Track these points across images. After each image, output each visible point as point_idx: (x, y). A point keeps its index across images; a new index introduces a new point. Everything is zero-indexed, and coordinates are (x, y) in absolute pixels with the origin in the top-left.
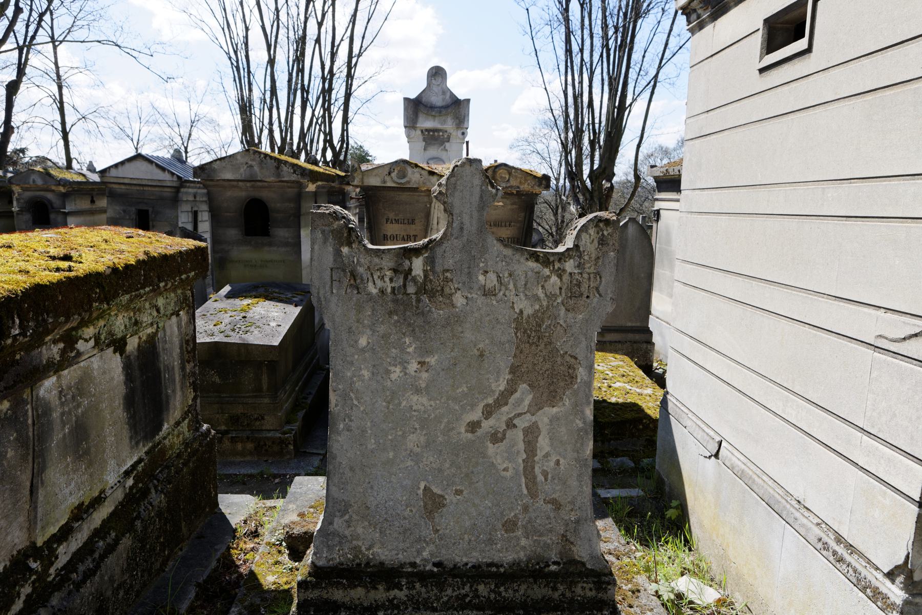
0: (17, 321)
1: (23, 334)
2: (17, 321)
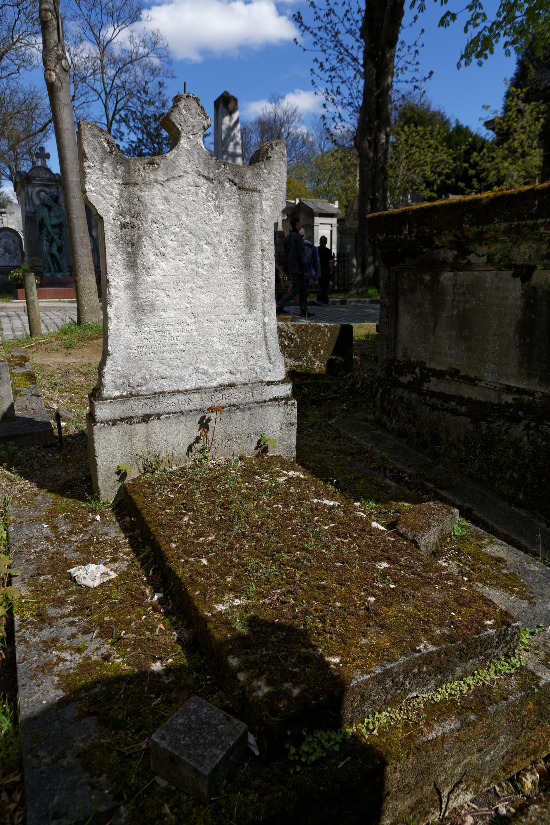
0: (407, 227)
1: (410, 233)
2: (407, 227)
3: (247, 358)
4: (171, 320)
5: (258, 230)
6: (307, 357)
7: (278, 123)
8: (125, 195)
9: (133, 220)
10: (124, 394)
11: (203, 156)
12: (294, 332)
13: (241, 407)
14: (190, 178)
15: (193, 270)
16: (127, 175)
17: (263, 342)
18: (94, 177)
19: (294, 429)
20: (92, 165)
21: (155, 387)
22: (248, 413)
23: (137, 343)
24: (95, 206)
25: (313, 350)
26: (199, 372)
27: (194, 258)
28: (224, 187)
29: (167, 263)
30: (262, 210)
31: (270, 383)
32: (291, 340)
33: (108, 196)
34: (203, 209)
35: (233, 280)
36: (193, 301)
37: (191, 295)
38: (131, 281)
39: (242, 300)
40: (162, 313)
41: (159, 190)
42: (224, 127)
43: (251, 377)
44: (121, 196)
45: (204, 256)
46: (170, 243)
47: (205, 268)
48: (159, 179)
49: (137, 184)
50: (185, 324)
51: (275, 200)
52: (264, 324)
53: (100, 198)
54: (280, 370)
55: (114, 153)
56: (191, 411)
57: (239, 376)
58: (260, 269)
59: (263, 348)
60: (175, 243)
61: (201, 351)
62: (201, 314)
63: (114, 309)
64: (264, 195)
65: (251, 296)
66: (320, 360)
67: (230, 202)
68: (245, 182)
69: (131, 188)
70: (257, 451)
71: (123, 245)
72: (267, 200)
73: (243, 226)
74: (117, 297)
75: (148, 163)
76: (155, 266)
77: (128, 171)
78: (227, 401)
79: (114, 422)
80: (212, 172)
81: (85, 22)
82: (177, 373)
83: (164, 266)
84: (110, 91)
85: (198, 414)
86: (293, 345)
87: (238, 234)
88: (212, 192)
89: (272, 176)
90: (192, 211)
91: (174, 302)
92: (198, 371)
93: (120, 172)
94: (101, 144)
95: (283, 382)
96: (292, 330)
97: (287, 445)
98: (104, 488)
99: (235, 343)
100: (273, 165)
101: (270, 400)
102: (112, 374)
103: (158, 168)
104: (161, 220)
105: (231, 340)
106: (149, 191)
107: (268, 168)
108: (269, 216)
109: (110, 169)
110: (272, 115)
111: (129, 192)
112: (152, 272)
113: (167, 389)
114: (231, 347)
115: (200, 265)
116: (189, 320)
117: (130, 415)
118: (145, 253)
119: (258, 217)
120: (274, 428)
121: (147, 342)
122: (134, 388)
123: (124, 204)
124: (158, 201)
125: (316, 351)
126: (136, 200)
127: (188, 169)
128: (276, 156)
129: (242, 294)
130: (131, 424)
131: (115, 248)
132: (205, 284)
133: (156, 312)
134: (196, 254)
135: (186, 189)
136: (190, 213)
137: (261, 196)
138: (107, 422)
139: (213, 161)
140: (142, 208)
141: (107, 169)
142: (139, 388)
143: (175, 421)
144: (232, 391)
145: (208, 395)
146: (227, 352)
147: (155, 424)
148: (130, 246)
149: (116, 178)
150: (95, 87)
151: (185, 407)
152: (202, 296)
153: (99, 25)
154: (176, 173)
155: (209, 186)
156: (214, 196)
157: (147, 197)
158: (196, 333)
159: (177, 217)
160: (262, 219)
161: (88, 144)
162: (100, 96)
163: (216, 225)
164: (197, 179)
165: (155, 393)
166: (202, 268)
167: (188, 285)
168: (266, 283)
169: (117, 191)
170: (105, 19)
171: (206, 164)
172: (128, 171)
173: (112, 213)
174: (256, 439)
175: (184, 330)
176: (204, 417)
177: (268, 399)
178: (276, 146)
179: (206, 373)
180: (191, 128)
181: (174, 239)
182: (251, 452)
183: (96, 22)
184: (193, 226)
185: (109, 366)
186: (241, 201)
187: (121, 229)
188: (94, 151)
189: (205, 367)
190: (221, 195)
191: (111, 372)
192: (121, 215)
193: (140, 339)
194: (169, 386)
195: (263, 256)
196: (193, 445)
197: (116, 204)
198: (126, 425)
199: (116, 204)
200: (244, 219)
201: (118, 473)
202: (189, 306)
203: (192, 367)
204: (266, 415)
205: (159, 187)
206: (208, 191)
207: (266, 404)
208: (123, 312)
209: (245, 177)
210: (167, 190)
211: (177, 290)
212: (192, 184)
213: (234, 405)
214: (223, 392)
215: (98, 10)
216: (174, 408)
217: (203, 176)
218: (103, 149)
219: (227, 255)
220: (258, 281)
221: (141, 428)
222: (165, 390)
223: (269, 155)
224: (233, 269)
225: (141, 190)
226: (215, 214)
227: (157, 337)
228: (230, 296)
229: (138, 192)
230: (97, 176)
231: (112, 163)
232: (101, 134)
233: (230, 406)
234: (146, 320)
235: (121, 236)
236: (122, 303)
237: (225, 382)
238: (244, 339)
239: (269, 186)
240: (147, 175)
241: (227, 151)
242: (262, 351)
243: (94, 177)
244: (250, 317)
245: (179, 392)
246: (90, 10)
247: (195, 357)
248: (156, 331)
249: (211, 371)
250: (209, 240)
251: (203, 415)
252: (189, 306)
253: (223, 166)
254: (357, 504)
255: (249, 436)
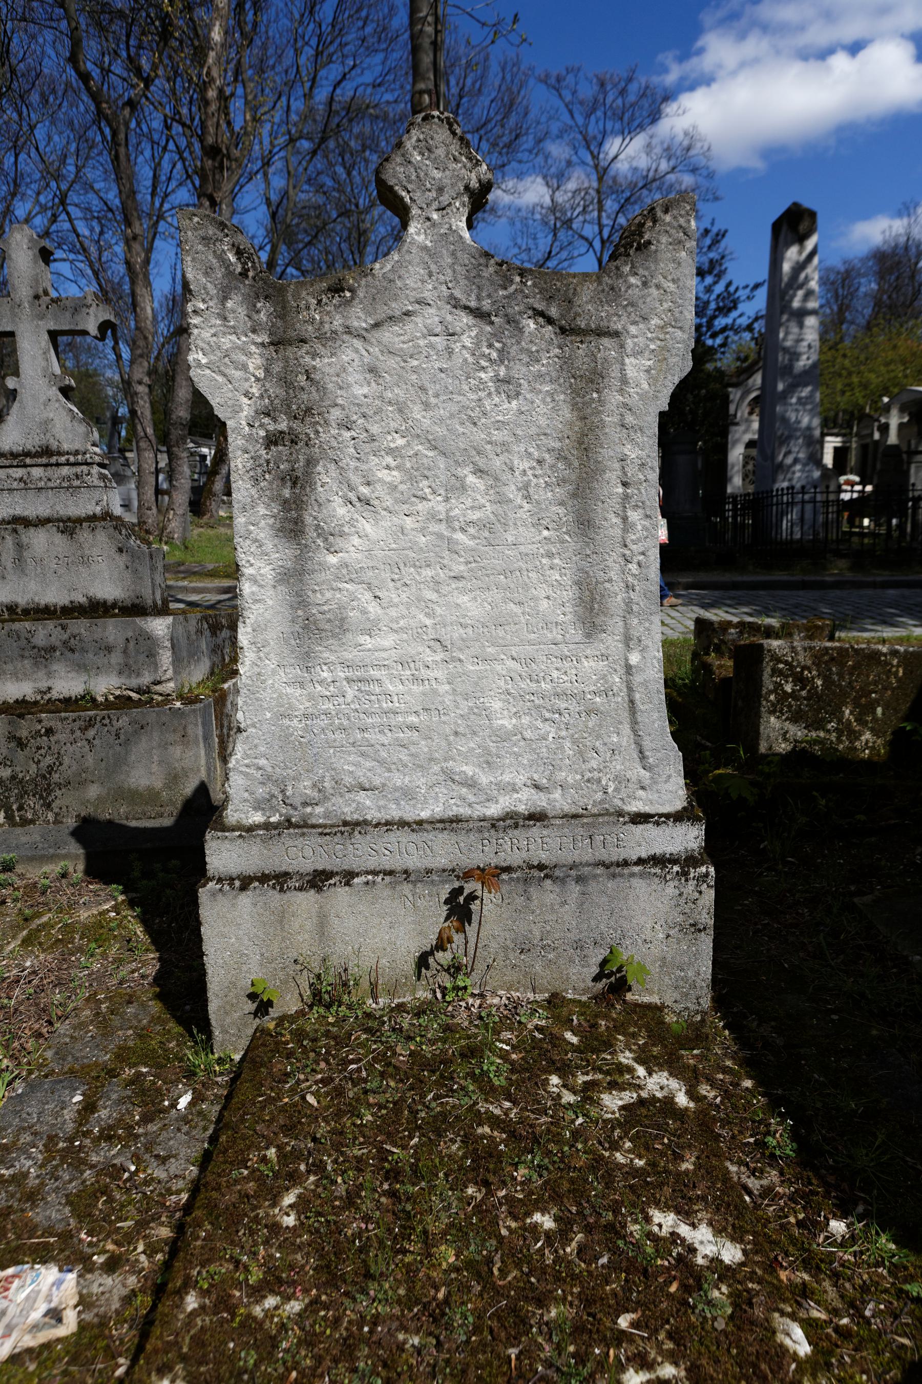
3: (581, 753)
4: (384, 655)
5: (613, 432)
6: (840, 721)
7: (914, 250)
8: (277, 368)
9: (295, 425)
10: (272, 820)
11: (465, 258)
12: (809, 663)
13: (558, 873)
14: (431, 317)
15: (440, 536)
16: (279, 323)
17: (625, 715)
18: (206, 334)
19: (706, 943)
20: (202, 306)
21: (346, 810)
22: (575, 889)
23: (303, 706)
24: (209, 398)
25: (856, 704)
26: (453, 781)
27: (441, 508)
28: (521, 330)
29: (377, 521)
30: (624, 381)
31: (640, 818)
32: (800, 680)
33: (238, 374)
34: (466, 388)
35: (544, 561)
36: (439, 611)
37: (434, 596)
38: (289, 564)
39: (569, 609)
40: (364, 639)
41: (357, 351)
42: (786, 267)
43: (592, 799)
44: (267, 371)
45: (469, 502)
46: (383, 474)
47: (472, 530)
48: (356, 324)
49: (303, 341)
50: (420, 665)
51: (661, 356)
52: (629, 668)
53: (220, 379)
54: (670, 786)
55: (251, 274)
56: (429, 871)
57: (557, 795)
58: (617, 532)
59: (626, 729)
60: (395, 473)
61: (461, 730)
62: (459, 643)
63: (249, 630)
64: (629, 343)
65: (593, 600)
66: (872, 730)
67: (535, 368)
68: (577, 315)
69: (290, 351)
70: (600, 985)
71: (271, 483)
72: (637, 354)
73: (571, 424)
74: (256, 601)
75: (329, 289)
76: (346, 529)
77: (283, 313)
78: (524, 855)
79: (245, 882)
80: (489, 296)
81: (580, 137)
82: (398, 780)
83: (367, 527)
84: (609, 237)
85: (443, 882)
86: (804, 693)
87: (557, 445)
88: (490, 346)
89: (654, 291)
90: (437, 396)
91: (393, 613)
92: (450, 777)
93: (263, 316)
94: (221, 258)
95: (677, 817)
96: (803, 658)
97: (685, 979)
98: (222, 1026)
99: (547, 715)
100: (656, 262)
101: (640, 861)
102: (246, 775)
103: (353, 298)
104: (360, 421)
105: (539, 707)
106: (332, 355)
107: (641, 271)
108: (643, 396)
109: (242, 311)
110: (903, 240)
111: (286, 360)
112: (339, 542)
113: (373, 815)
114: (539, 723)
115: (456, 525)
116: (429, 657)
117: (284, 868)
118: (322, 498)
119: (614, 398)
120: (648, 935)
121: (327, 706)
122: (296, 809)
123: (275, 390)
124: (353, 377)
125: (864, 710)
126: (302, 378)
127: (426, 294)
128: (664, 239)
129: (569, 594)
130: (281, 890)
131: (253, 491)
132: (471, 570)
133: (349, 636)
134: (447, 499)
135: (422, 342)
136: (433, 400)
137: (622, 346)
138: (232, 879)
139: (491, 269)
140: (315, 395)
141: (234, 312)
142: (309, 810)
143: (387, 892)
144: (536, 831)
145: (472, 837)
146: (528, 734)
147: (339, 897)
148: (289, 484)
149: (254, 331)
150: (584, 233)
151: (414, 861)
152: (464, 599)
153: (600, 137)
154: (396, 308)
155: (481, 331)
156: (494, 355)
157: (327, 370)
158: (447, 687)
159: (400, 411)
160: (625, 405)
161: (193, 260)
162: (591, 245)
163: (500, 425)
164: (449, 318)
165: (345, 823)
166: (463, 530)
167: (428, 573)
168: (633, 567)
169: (259, 361)
170: (609, 126)
171: (474, 278)
172: (283, 313)
173: (247, 409)
174: (601, 954)
175: (415, 679)
176: (460, 890)
177: (635, 858)
178: (666, 211)
179: (471, 784)
180: (433, 194)
181: (393, 464)
182: (582, 985)
183: (596, 131)
184: (440, 431)
185: (239, 756)
186: (566, 362)
187: (267, 447)
188: (206, 274)
189: (469, 770)
190: (514, 350)
191: (244, 769)
192: (268, 415)
193: (311, 697)
194: (379, 809)
195: (626, 497)
196: (431, 953)
197: (255, 391)
198: (271, 892)
199: (255, 391)
200: (574, 406)
201: (252, 996)
202: (428, 622)
203: (436, 768)
204: (626, 899)
205: (357, 343)
206: (478, 345)
207: (626, 871)
208: (271, 635)
209: (577, 301)
210: (375, 350)
211: (399, 584)
212: (438, 330)
213: (541, 867)
214: (512, 833)
215: (599, 113)
216: (387, 863)
217: (466, 308)
218: (227, 268)
219: (528, 497)
220: (613, 560)
221: (306, 901)
222: (369, 817)
223: (647, 237)
224: (546, 533)
225: (314, 355)
226: (497, 400)
227: (350, 693)
228: (534, 599)
229: (308, 359)
230: (213, 331)
231: (246, 297)
232: (220, 235)
233: (531, 867)
234: (325, 655)
235: (268, 462)
236: (267, 615)
237: (522, 809)
238: (574, 707)
239: (645, 319)
240: (327, 319)
241: (790, 307)
242: (623, 738)
243: (206, 334)
244: (588, 652)
245: (403, 824)
246: (588, 116)
247: (444, 743)
248: (349, 680)
249: (484, 779)
250: (481, 462)
251: (457, 885)
252: (428, 622)
253: (518, 279)
254: (838, 1227)
255: (578, 945)
